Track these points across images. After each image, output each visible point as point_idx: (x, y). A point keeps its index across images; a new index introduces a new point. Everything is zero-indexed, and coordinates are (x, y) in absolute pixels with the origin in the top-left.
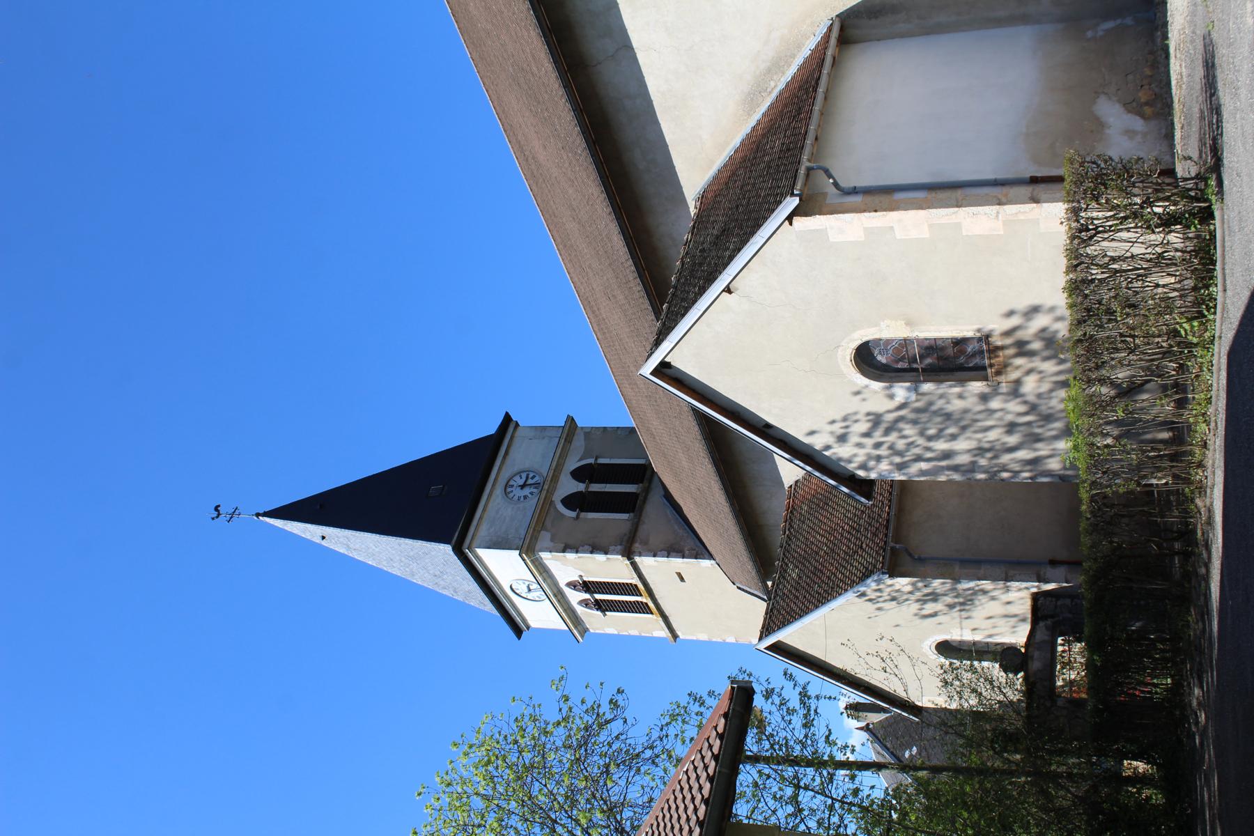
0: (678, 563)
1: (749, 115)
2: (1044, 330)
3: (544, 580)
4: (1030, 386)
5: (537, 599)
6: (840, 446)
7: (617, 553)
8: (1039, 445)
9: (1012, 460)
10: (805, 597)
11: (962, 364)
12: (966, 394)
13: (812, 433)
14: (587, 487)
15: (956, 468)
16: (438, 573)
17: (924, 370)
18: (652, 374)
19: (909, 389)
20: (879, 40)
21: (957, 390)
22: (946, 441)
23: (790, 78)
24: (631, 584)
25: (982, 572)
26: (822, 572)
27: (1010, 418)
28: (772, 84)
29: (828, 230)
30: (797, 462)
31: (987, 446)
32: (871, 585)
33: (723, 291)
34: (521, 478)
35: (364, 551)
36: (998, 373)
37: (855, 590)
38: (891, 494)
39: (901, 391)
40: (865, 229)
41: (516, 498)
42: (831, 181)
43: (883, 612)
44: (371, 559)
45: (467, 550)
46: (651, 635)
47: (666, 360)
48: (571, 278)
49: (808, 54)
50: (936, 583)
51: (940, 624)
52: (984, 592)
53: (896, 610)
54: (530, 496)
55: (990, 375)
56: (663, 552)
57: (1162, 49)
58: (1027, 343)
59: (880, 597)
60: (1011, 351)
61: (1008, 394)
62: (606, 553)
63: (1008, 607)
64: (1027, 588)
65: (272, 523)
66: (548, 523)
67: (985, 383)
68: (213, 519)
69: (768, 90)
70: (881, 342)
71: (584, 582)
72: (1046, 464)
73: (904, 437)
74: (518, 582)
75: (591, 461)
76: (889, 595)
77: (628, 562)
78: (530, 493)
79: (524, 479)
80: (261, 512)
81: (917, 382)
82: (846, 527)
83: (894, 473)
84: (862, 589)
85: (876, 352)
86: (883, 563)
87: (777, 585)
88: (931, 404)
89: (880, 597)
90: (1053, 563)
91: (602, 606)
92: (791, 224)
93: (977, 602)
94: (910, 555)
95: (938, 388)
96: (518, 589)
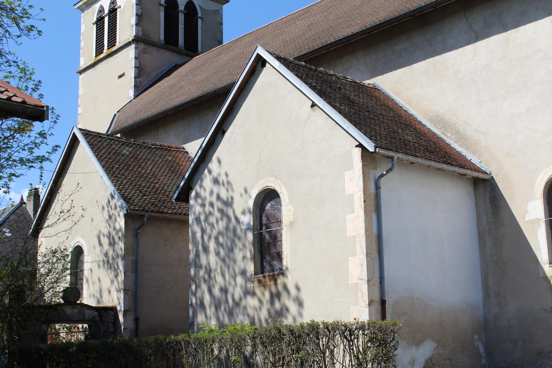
0: (131, 74)
2: (287, 310)
4: (252, 302)
7: (137, 32)
8: (213, 309)
9: (203, 291)
10: (110, 159)
11: (265, 258)
12: (246, 261)
13: (219, 161)
14: (181, 12)
15: (197, 255)
17: (261, 234)
18: (258, 54)
19: (249, 224)
20: (476, 204)
21: (248, 255)
22: (215, 249)
23: (453, 146)
27: (231, 289)
29: (353, 171)
30: (200, 152)
31: (212, 275)
32: (119, 202)
33: (313, 102)
36: (260, 282)
37: (116, 192)
38: (180, 214)
39: (247, 219)
42: (385, 173)
46: (81, 56)
49: (468, 158)
50: (121, 245)
51: (94, 248)
52: (116, 276)
55: (258, 276)
56: (138, 64)
58: (279, 299)
59: (111, 208)
60: (274, 289)
62: (136, 25)
63: (107, 292)
64: (119, 303)
67: (253, 273)
69: (445, 132)
71: (116, 10)
73: (217, 222)
75: (200, 15)
77: (130, 40)
81: (253, 229)
83: (194, 216)
84: (116, 196)
85: (272, 203)
86: (134, 209)
87: (117, 140)
88: (239, 239)
89: (111, 208)
90: (137, 320)
92: (357, 146)
93: (109, 271)
94: (140, 227)
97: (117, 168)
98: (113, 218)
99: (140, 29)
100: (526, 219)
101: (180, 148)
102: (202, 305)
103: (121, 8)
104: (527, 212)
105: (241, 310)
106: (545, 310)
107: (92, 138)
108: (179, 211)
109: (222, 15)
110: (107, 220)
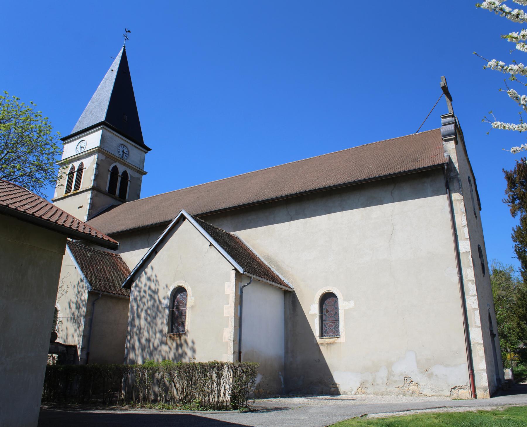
0: (87, 207)
1: (263, 257)
2: (186, 354)
3: (85, 154)
4: (165, 348)
5: (77, 150)
6: (146, 278)
7: (94, 184)
8: (140, 350)
9: (135, 340)
10: (81, 258)
11: (174, 324)
12: (163, 325)
13: (152, 268)
14: (120, 176)
15: (133, 319)
16: (92, 112)
17: (173, 311)
18: (182, 214)
19: (167, 305)
20: (284, 303)
21: (165, 322)
22: (145, 317)
23: (275, 272)
24: (80, 187)
25: (87, 327)
26: (90, 265)
27: (152, 340)
28: (273, 266)
29: (230, 282)
30: (141, 262)
31: (142, 331)
32: (85, 284)
33: (211, 243)
34: (126, 151)
35: (105, 85)
36: (170, 337)
37: (85, 278)
38: (119, 294)
39: (166, 302)
40: (229, 295)
41: (119, 148)
42: (246, 285)
43: (73, 288)
44: (101, 87)
45: (102, 127)
46: (55, 191)
47: (186, 220)
48: (204, 184)
49: (282, 279)
50: (84, 309)
51: (66, 309)
52: (79, 327)
53: (74, 293)
54: (119, 154)
55: (170, 334)
56: (92, 202)
57: (276, 396)
58: (182, 348)
59: (80, 287)
60: (179, 342)
61: (162, 340)
62: (94, 180)
63: (71, 336)
64: (79, 343)
65: (121, 51)
66: (108, 159)
67: (167, 332)
68: (125, 29)
69: (271, 265)
70: (185, 297)
71: (82, 169)
72: (132, 353)
73: (148, 302)
74: (86, 144)
75: (129, 179)
76: (80, 291)
77: (89, 188)
78: (120, 154)
79: (126, 152)
80: (126, 48)
81: (169, 308)
82: (106, 276)
83: (133, 297)
84: (85, 281)
85: (181, 294)
86: (94, 289)
87: (84, 248)
88: (160, 312)
89: (80, 287)
90: (88, 354)
91: (71, 174)
92: (233, 269)
93: (74, 324)
94: (96, 300)
95: (166, 315)
96: (82, 143)
97: (85, 264)
98: (81, 293)
99: (96, 183)
100: (310, 314)
101: (118, 255)
102: (133, 348)
103: (86, 169)
104: (310, 310)
105: (158, 352)
106: (316, 360)
107: (71, 245)
108: (119, 292)
109: (141, 181)
110: (76, 294)
